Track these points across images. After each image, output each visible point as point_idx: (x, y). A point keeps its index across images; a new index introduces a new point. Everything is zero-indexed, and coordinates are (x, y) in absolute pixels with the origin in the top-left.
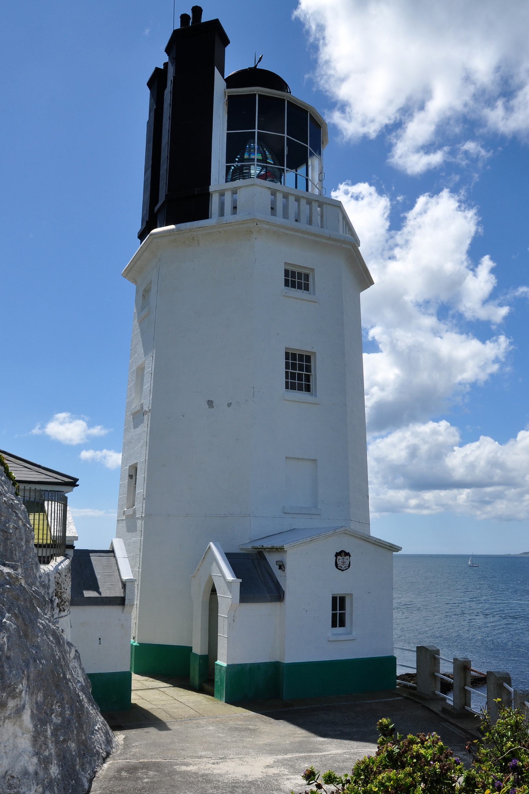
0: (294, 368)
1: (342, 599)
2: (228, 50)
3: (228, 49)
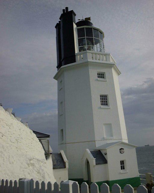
1: (123, 161)
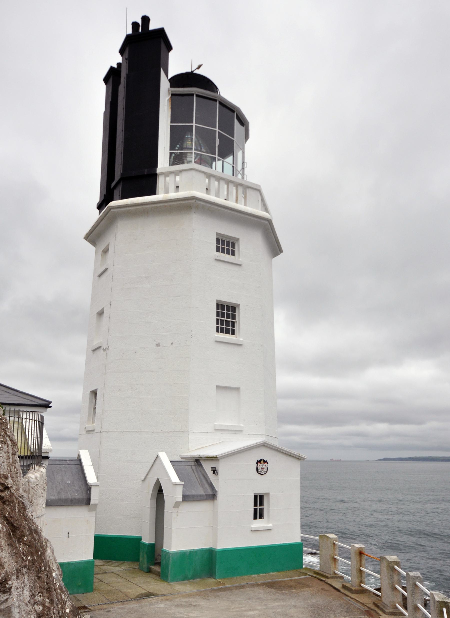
0: (223, 316)
1: (261, 497)
2: (171, 54)
3: (171, 54)
